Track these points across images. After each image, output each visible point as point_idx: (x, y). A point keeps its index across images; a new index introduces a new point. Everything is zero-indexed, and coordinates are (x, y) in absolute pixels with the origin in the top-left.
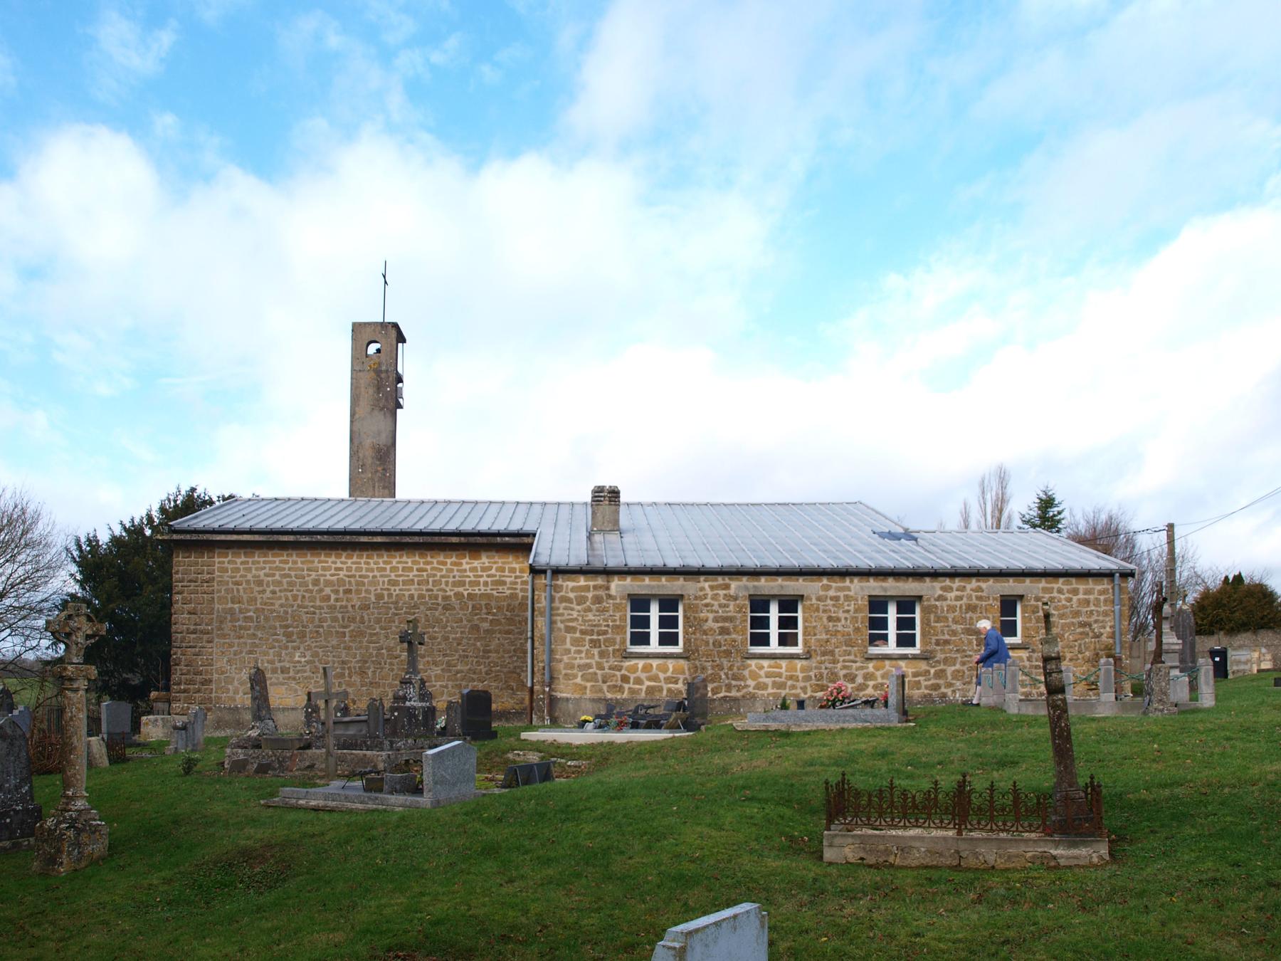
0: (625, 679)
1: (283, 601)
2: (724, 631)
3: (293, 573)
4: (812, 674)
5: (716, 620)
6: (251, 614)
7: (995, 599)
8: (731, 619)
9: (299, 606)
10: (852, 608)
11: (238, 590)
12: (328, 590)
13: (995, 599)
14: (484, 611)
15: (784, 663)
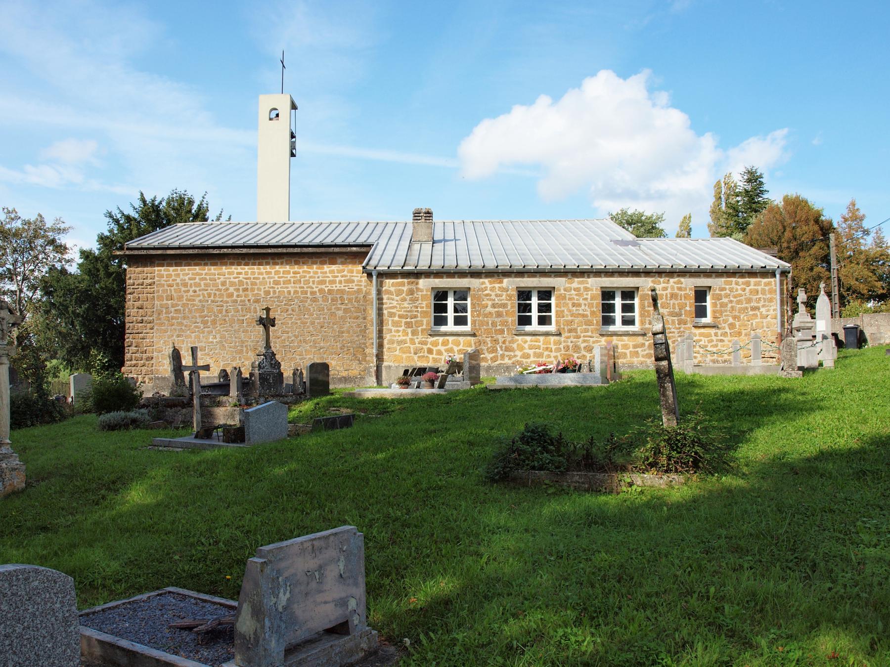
0: (430, 351)
1: (201, 297)
2: (499, 315)
3: (208, 277)
4: (562, 346)
5: (494, 306)
6: (179, 307)
7: (690, 289)
8: (504, 306)
9: (213, 301)
10: (589, 297)
11: (171, 291)
12: (231, 289)
13: (690, 289)
14: (340, 302)
15: (542, 338)
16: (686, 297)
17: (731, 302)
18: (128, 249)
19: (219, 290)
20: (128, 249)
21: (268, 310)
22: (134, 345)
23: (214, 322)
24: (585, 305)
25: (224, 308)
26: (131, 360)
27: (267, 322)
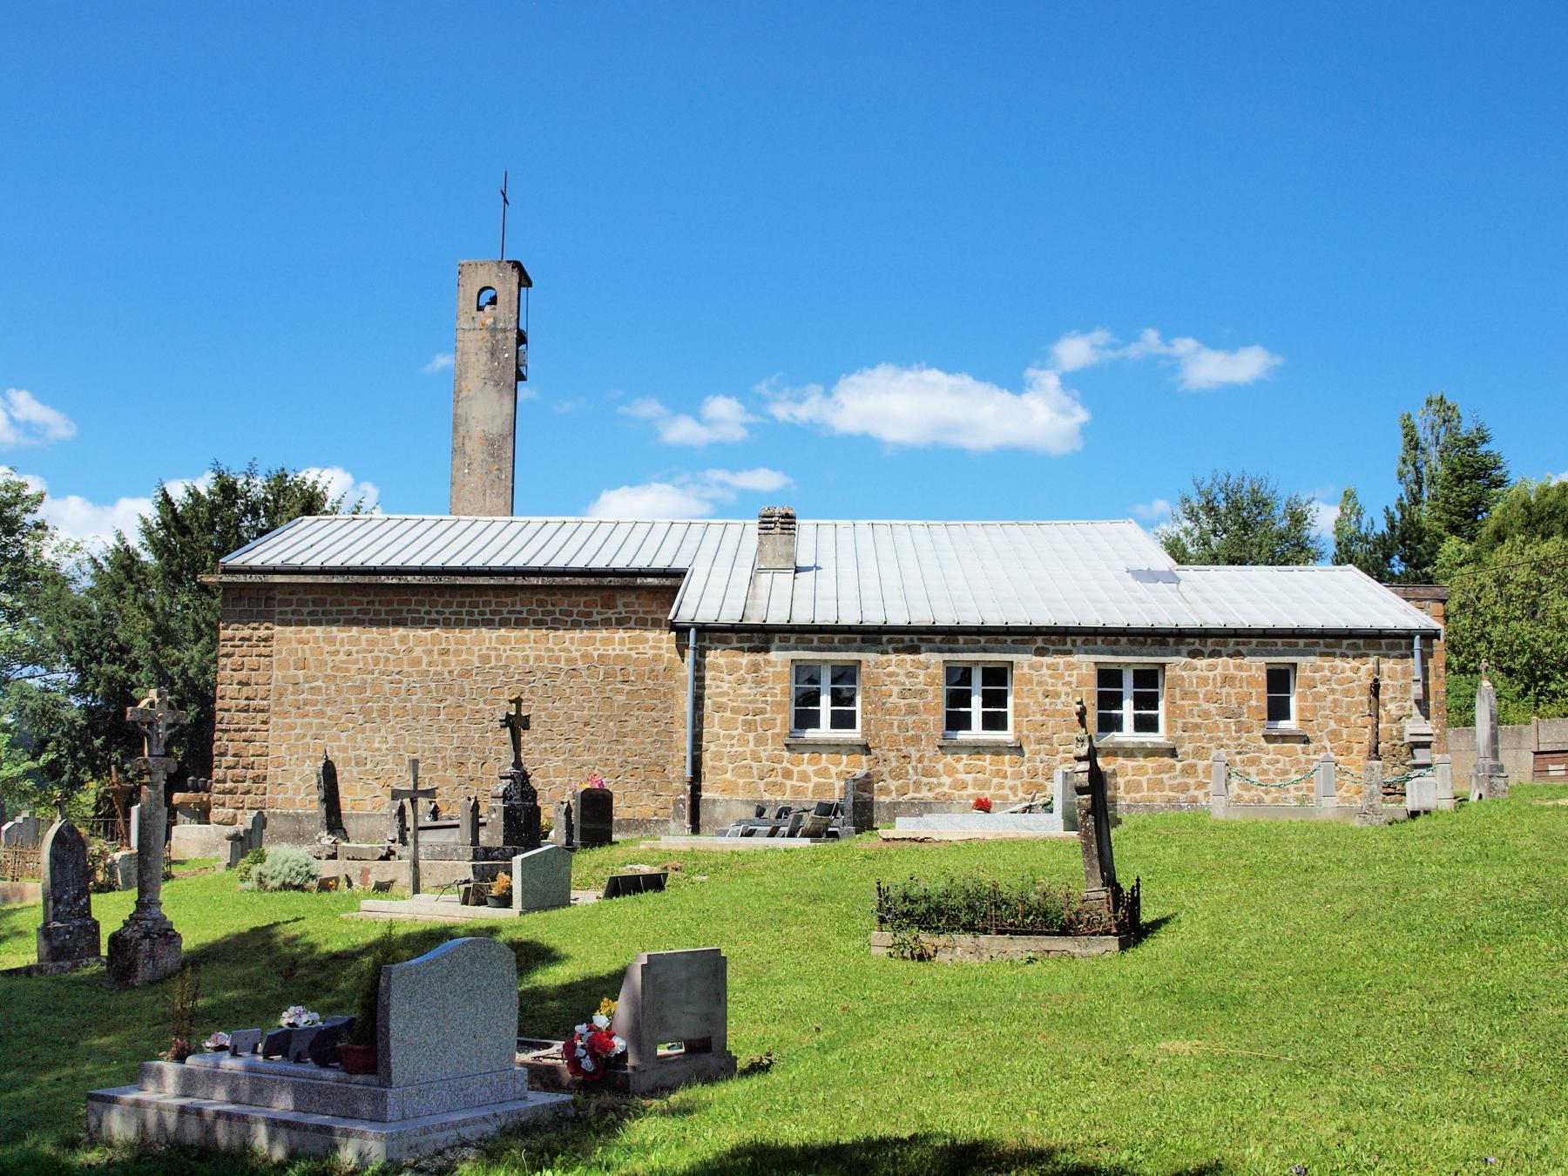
0: (787, 774)
2: (912, 710)
8: (921, 693)
9: (382, 673)
10: (1074, 680)
11: (303, 651)
12: (418, 651)
16: (1251, 681)
17: (1333, 691)
18: (226, 571)
19: (394, 651)
20: (226, 571)
21: (518, 702)
22: (230, 752)
23: (384, 712)
24: (1067, 694)
25: (404, 686)
26: (224, 781)
27: (516, 724)
